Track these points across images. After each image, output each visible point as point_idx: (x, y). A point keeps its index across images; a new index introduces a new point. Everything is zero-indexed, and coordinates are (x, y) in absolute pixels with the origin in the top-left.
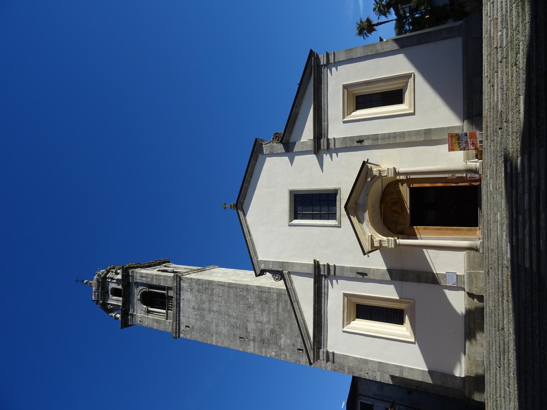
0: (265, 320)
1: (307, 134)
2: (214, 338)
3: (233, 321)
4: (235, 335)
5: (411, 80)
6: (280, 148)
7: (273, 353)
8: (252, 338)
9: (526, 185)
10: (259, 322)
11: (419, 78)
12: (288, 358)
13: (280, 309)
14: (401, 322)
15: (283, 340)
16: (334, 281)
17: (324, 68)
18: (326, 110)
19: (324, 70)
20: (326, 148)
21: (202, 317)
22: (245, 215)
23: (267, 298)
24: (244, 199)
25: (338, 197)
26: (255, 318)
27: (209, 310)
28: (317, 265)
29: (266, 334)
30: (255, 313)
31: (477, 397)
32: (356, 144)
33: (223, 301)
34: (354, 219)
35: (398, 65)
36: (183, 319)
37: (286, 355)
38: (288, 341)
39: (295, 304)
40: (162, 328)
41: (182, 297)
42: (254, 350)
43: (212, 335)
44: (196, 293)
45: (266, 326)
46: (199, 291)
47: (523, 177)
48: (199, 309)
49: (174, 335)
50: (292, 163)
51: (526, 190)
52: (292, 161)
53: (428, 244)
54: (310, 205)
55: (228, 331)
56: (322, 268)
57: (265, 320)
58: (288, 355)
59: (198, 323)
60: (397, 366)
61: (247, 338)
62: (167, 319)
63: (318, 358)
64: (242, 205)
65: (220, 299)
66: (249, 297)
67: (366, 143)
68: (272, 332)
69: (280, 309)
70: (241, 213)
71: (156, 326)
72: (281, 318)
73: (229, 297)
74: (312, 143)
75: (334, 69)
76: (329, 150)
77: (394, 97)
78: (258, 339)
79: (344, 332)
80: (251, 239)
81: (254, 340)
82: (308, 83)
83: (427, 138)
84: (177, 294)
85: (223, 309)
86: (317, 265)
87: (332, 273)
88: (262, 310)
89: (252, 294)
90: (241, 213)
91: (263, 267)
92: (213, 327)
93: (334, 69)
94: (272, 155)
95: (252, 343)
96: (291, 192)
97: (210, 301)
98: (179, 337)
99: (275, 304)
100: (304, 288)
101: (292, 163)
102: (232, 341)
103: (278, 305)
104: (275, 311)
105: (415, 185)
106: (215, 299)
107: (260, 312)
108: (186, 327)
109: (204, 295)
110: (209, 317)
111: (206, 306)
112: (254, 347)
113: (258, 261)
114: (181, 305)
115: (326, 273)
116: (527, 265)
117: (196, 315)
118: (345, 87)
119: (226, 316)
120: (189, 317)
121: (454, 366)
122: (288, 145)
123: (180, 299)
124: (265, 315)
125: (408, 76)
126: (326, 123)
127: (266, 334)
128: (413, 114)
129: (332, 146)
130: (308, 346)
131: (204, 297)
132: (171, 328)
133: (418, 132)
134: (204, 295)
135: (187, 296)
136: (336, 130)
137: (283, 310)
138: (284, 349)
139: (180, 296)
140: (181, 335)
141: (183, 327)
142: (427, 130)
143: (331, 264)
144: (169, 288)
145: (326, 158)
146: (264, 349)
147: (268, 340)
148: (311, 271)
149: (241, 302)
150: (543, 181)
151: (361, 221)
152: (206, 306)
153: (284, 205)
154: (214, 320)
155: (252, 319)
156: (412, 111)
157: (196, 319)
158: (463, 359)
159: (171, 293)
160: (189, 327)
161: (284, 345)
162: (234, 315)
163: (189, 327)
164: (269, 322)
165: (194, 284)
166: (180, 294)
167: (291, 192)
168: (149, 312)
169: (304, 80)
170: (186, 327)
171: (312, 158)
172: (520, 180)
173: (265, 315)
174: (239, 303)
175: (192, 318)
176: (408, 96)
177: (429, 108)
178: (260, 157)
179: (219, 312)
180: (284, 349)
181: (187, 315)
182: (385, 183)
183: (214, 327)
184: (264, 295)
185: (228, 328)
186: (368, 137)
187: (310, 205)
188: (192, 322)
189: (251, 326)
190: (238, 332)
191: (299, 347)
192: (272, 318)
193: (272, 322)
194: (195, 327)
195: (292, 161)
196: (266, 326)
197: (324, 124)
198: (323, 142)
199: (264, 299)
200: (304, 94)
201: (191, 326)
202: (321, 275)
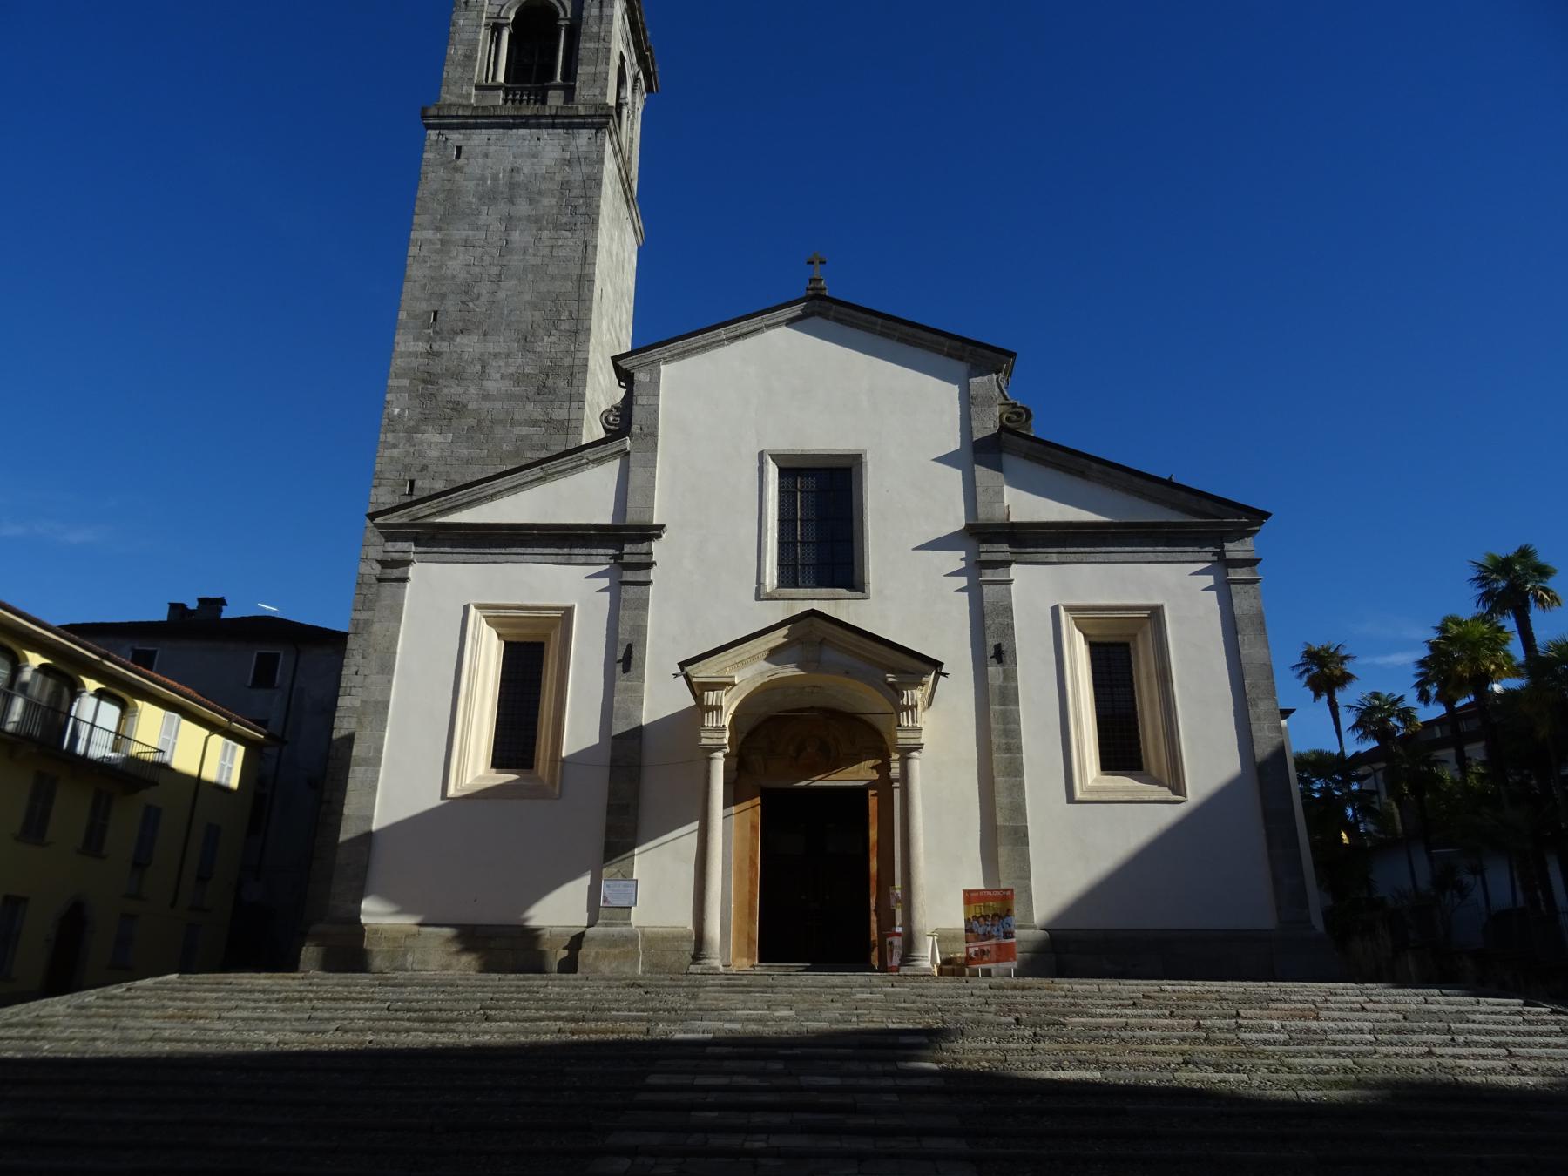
0: (491, 386)
1: (1023, 505)
2: (429, 234)
3: (484, 289)
4: (443, 296)
5: (1166, 793)
6: (987, 425)
7: (397, 411)
8: (436, 347)
9: (864, 1082)
10: (484, 367)
11: (1168, 815)
12: (387, 453)
13: (525, 430)
14: (500, 760)
15: (438, 438)
16: (605, 582)
17: (1214, 554)
18: (1091, 558)
19: (1208, 552)
20: (984, 557)
21: (489, 198)
22: (790, 323)
23: (552, 391)
24: (836, 320)
25: (843, 592)
26: (496, 355)
27: (510, 218)
28: (651, 532)
29: (452, 390)
30: (508, 356)
31: (309, 953)
32: (992, 642)
33: (538, 261)
34: (778, 638)
35: (1209, 756)
36: (479, 137)
37: (395, 446)
38: (435, 454)
39: (537, 472)
40: (451, 72)
41: (544, 133)
42: (402, 355)
43: (438, 229)
44: (558, 178)
45: (473, 390)
46: (565, 185)
47: (885, 1074)
48: (512, 186)
49: (433, 111)
50: (940, 460)
51: (850, 1081)
52: (946, 460)
53: (710, 835)
54: (821, 512)
55: (454, 277)
56: (643, 547)
57: (491, 386)
58: (395, 453)
59: (471, 185)
60: (379, 750)
61: (436, 333)
62: (478, 87)
63: (390, 537)
64: (820, 314)
65: (546, 251)
66: (553, 339)
67: (994, 670)
68: (458, 408)
69: (525, 430)
70: (796, 311)
71: (456, 51)
72: (499, 431)
73: (553, 278)
74: (998, 517)
75: (1209, 580)
76: (976, 568)
77: (1122, 747)
78: (437, 366)
79: (466, 609)
80: (720, 343)
81: (432, 354)
82: (1174, 506)
83: (1002, 833)
84: (554, 117)
85: (515, 261)
86: (651, 532)
87: (629, 576)
88: (518, 378)
89: (562, 347)
90: (796, 311)
91: (641, 377)
92: (460, 232)
93: (1209, 580)
94: (967, 401)
95: (421, 347)
96: (857, 459)
97: (537, 220)
98: (429, 127)
99: (538, 415)
100: (584, 497)
101: (940, 460)
102: (424, 287)
103: (534, 423)
104: (518, 416)
105: (873, 803)
106: (545, 234)
107: (512, 369)
108: (459, 149)
109: (553, 201)
110: (490, 217)
111: (523, 208)
112: (411, 354)
113: (656, 362)
114: (522, 131)
115: (626, 559)
116: (653, 1080)
117: (495, 178)
118: (1156, 613)
119: (495, 270)
120: (486, 156)
121: (386, 895)
122: (990, 450)
123: (539, 126)
124: (506, 385)
125: (1177, 786)
126: (1054, 558)
127: (452, 390)
128: (1071, 799)
129: (989, 575)
130: (421, 510)
131: (549, 201)
132: (454, 99)
133: (1019, 810)
134: (553, 201)
135: (548, 148)
136: (1034, 588)
137: (521, 438)
138: (409, 440)
139: (547, 126)
140: (432, 134)
141: (456, 137)
142: (1026, 835)
143: (653, 574)
144: (569, 93)
145: (955, 559)
146: (406, 382)
147: (433, 396)
148: (633, 517)
149: (538, 315)
150: (837, 1144)
151: (774, 655)
152: (523, 208)
153: (821, 438)
154: (482, 234)
155: (491, 347)
156: (1078, 795)
157: (483, 179)
158: (407, 921)
159: (555, 99)
160: (458, 156)
161: (422, 443)
162: (501, 295)
163: (458, 156)
164: (486, 397)
165: (586, 169)
166: (554, 126)
167: (857, 459)
168: (496, 29)
169: (1183, 495)
170: (459, 149)
171: (955, 520)
172: (878, 1067)
173: (506, 385)
174: (535, 307)
175: (484, 167)
176: (1123, 784)
177: (1083, 837)
178: (961, 367)
179: (506, 248)
180: (409, 440)
181: (492, 149)
182: (880, 723)
183: (464, 234)
184: (562, 383)
185: (462, 276)
186: (1010, 676)
187: (821, 512)
188: (474, 167)
189: (470, 345)
190: (451, 306)
191: (418, 483)
192: (498, 405)
193: (486, 405)
194: (458, 176)
195: (946, 460)
196: (473, 390)
197: (1053, 553)
198: (1002, 550)
199: (550, 382)
200: (1142, 495)
201: (461, 162)
202: (623, 544)
